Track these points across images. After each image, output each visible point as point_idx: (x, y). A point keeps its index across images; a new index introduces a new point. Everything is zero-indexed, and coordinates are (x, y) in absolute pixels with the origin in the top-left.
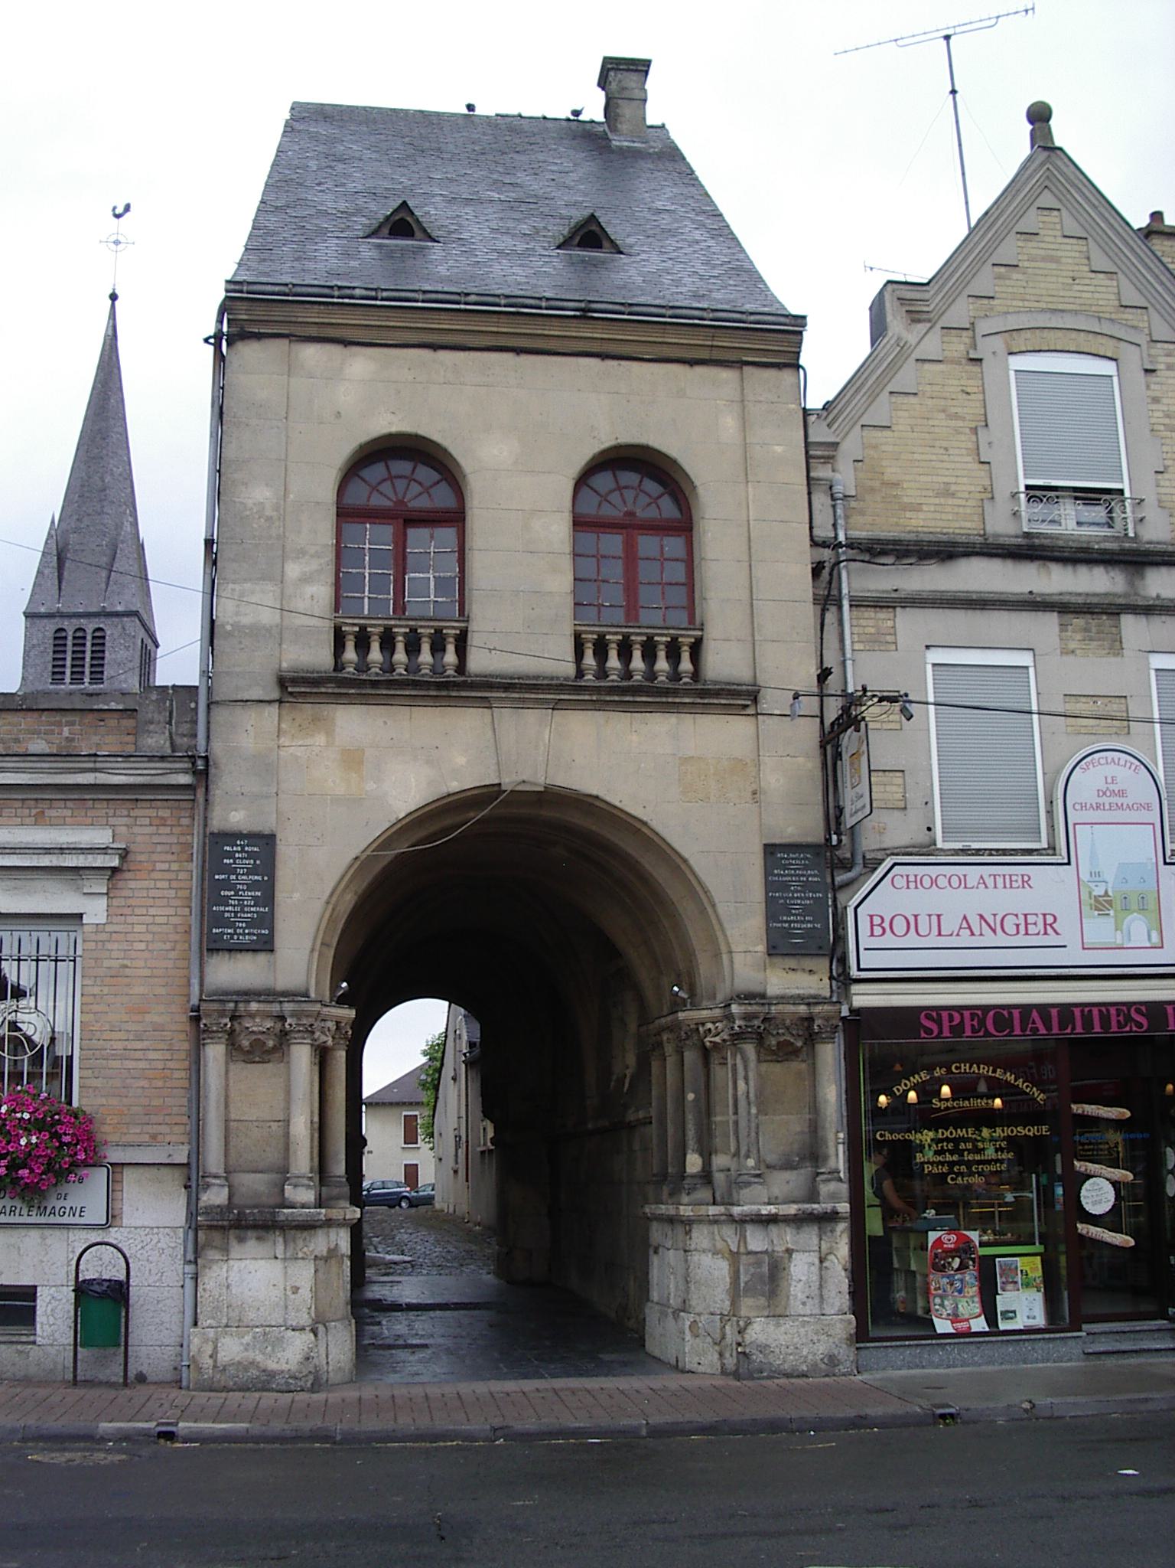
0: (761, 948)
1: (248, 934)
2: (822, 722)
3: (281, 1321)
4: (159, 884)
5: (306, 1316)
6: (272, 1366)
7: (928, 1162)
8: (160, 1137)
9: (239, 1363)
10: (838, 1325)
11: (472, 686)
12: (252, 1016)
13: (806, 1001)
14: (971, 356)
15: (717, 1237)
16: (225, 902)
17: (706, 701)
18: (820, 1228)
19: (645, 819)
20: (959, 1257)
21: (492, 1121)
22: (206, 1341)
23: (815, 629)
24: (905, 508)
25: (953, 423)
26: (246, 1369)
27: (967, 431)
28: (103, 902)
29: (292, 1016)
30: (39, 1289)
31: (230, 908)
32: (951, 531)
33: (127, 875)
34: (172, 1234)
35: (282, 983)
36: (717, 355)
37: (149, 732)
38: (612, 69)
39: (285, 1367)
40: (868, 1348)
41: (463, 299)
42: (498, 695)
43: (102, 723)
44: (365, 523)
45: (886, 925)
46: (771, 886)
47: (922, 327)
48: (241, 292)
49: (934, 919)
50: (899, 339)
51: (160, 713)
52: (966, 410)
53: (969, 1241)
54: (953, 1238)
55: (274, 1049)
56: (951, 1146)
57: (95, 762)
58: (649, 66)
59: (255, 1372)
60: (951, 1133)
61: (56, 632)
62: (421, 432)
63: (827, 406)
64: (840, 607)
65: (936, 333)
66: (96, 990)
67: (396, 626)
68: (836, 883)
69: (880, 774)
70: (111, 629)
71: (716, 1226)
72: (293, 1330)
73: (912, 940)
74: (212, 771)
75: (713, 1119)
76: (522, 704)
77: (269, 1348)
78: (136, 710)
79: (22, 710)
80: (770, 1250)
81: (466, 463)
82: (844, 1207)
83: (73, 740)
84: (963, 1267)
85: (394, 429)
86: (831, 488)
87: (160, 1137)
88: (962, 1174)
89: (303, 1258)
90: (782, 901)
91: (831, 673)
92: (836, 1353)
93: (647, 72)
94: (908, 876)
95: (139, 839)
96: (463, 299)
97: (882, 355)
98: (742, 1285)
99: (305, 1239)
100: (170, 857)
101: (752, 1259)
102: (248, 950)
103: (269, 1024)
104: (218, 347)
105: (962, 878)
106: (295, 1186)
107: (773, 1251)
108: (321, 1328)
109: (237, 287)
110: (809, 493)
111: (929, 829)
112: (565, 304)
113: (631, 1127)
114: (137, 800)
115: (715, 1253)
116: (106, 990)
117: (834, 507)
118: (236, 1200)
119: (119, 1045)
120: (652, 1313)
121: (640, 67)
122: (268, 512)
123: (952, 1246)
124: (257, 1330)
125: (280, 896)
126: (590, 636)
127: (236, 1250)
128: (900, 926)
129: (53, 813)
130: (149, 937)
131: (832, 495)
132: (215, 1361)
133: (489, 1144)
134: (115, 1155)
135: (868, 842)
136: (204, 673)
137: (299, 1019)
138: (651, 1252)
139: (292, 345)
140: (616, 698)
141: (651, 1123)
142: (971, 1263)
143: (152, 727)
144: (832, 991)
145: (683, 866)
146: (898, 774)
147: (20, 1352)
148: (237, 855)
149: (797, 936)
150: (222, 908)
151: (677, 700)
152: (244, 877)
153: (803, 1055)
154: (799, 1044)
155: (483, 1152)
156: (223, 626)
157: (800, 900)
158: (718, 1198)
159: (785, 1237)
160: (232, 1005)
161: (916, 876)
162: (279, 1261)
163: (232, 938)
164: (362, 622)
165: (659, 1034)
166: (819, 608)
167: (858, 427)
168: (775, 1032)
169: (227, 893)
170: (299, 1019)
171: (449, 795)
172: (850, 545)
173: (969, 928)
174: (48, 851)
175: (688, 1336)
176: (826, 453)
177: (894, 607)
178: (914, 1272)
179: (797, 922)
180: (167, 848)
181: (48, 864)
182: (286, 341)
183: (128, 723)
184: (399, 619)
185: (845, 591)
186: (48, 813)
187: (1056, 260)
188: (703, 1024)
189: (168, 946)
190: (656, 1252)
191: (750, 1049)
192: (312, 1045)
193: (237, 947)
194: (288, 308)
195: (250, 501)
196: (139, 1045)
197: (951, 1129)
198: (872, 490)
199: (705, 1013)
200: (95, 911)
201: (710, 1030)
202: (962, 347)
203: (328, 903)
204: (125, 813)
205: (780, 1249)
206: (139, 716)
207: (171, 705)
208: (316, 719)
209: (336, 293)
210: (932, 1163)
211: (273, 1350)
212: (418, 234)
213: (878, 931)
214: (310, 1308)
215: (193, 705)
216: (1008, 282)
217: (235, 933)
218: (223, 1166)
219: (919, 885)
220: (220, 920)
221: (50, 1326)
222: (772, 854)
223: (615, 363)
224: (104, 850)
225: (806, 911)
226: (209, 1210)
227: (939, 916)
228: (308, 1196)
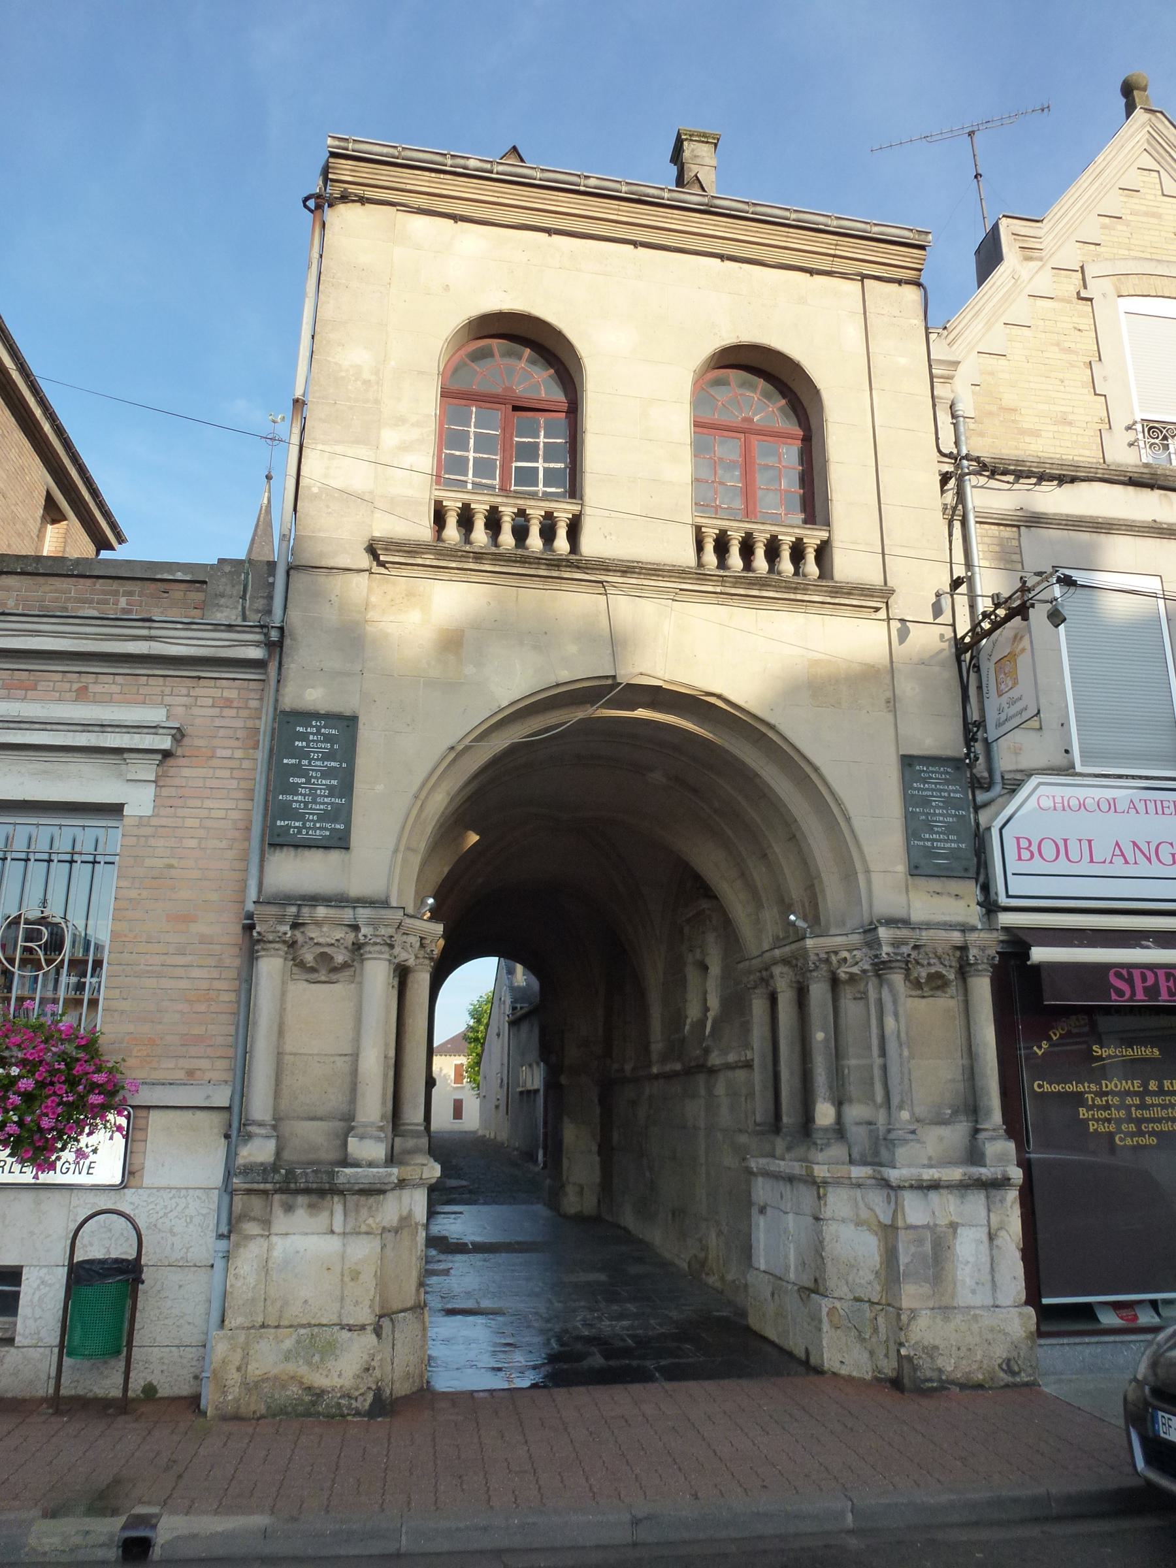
0: (901, 868)
1: (319, 828)
3: (335, 1320)
4: (219, 773)
5: (367, 1310)
6: (320, 1380)
8: (198, 1072)
9: (276, 1378)
12: (318, 924)
14: (1082, 295)
15: (861, 1205)
16: (293, 789)
17: (837, 601)
18: (987, 1197)
24: (1023, 432)
26: (284, 1387)
28: (151, 790)
30: (25, 1271)
31: (300, 798)
33: (181, 761)
34: (204, 1197)
35: (356, 889)
38: (686, 139)
43: (166, 595)
44: (469, 406)
45: (1034, 848)
46: (910, 800)
49: (1085, 845)
52: (1079, 346)
56: (1116, 1101)
57: (150, 628)
59: (294, 1390)
60: (1116, 1086)
65: (1047, 273)
66: (133, 894)
71: (859, 1190)
72: (350, 1330)
73: (1062, 866)
74: (287, 642)
75: (846, 1062)
78: (205, 582)
80: (931, 1224)
81: (583, 348)
87: (198, 1072)
89: (367, 1233)
94: (1054, 797)
95: (197, 722)
97: (998, 283)
98: (902, 1268)
101: (911, 1235)
102: (318, 847)
103: (339, 934)
106: (362, 1138)
107: (936, 1225)
111: (1067, 751)
114: (199, 678)
115: (859, 1223)
116: (145, 893)
118: (286, 1155)
122: (366, 375)
124: (302, 1331)
125: (360, 787)
126: (711, 530)
128: (1049, 850)
129: (98, 688)
130: (202, 833)
134: (145, 1097)
135: (1005, 762)
137: (376, 929)
138: (754, 1211)
140: (742, 592)
143: (222, 601)
145: (814, 776)
149: (939, 856)
150: (290, 798)
151: (806, 598)
152: (318, 763)
153: (952, 990)
156: (309, 488)
158: (855, 1155)
159: (946, 1207)
160: (293, 910)
161: (1062, 797)
162: (335, 1237)
163: (300, 832)
167: (1000, 324)
168: (925, 962)
169: (297, 780)
170: (376, 929)
171: (558, 685)
173: (1123, 855)
174: (86, 727)
175: (826, 1327)
180: (230, 732)
183: (196, 596)
186: (92, 688)
187: (1158, 216)
188: (836, 953)
189: (224, 844)
190: (762, 1210)
191: (897, 978)
192: (389, 961)
196: (181, 960)
197: (1115, 1080)
198: (991, 414)
199: (839, 940)
201: (845, 959)
203: (416, 797)
204: (184, 691)
206: (209, 588)
210: (1097, 1120)
211: (322, 1360)
213: (1026, 855)
216: (1112, 232)
217: (304, 827)
218: (271, 1112)
220: (286, 811)
221: (36, 1320)
222: (910, 765)
224: (154, 729)
225: (949, 830)
226: (247, 1170)
227: (1090, 841)
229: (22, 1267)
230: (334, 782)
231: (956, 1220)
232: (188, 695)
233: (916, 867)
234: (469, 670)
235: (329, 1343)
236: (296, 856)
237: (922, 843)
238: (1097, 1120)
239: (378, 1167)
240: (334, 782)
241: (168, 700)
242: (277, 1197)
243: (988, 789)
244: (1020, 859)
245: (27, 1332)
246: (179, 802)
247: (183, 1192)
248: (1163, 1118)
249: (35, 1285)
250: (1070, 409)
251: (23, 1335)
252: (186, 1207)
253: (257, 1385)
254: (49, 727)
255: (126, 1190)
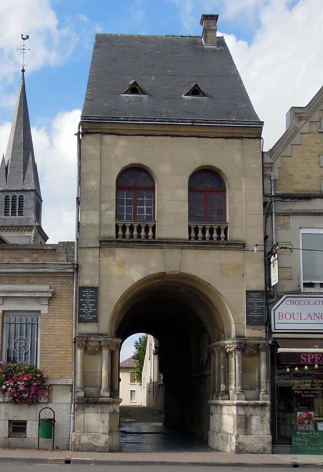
1: (90, 317)
2: (265, 252)
6: (96, 444)
7: (296, 390)
10: (266, 439)
11: (158, 242)
12: (92, 341)
13: (258, 339)
15: (230, 410)
19: (209, 283)
20: (307, 420)
21: (162, 374)
22: (77, 437)
23: (264, 223)
24: (295, 183)
25: (312, 154)
27: (317, 156)
28: (47, 307)
29: (103, 341)
30: (27, 421)
31: (85, 309)
32: (309, 190)
33: (54, 299)
36: (234, 135)
37: (60, 256)
39: (100, 445)
40: (276, 446)
41: (154, 120)
42: (165, 245)
44: (124, 191)
45: (284, 316)
47: (303, 122)
48: (86, 119)
49: (299, 314)
50: (295, 127)
51: (63, 250)
53: (310, 415)
54: (305, 414)
55: (97, 352)
58: (218, 17)
61: (6, 197)
62: (141, 163)
63: (271, 151)
64: (272, 216)
66: (45, 333)
67: (134, 224)
68: (268, 303)
69: (284, 268)
70: (26, 196)
71: (229, 407)
73: (292, 321)
74: (79, 268)
76: (171, 248)
77: (96, 439)
78: (56, 249)
79: (22, 249)
80: (245, 414)
82: (268, 402)
83: (37, 258)
84: (309, 423)
85: (133, 162)
86: (270, 177)
88: (307, 394)
89: (106, 413)
90: (251, 308)
91: (268, 237)
92: (265, 447)
93: (217, 19)
94: (291, 301)
96: (154, 120)
99: (106, 407)
100: (66, 294)
103: (96, 344)
104: (79, 137)
105: (309, 301)
107: (246, 415)
108: (111, 434)
109: (84, 118)
110: (263, 180)
111: (299, 286)
112: (186, 121)
113: (206, 376)
114: (57, 276)
117: (271, 183)
119: (51, 349)
120: (210, 434)
121: (214, 18)
123: (305, 417)
127: (86, 410)
128: (288, 316)
129: (32, 280)
130: (60, 317)
131: (271, 180)
132: (80, 443)
133: (161, 382)
136: (78, 239)
138: (211, 414)
139: (102, 136)
141: (211, 375)
142: (311, 422)
143: (61, 254)
144: (266, 336)
146: (289, 268)
147: (22, 440)
148: (87, 293)
150: (83, 309)
152: (89, 300)
154: (255, 352)
155: (159, 385)
157: (257, 307)
161: (294, 301)
163: (85, 318)
164: (124, 222)
165: (214, 347)
166: (265, 216)
169: (84, 305)
172: (276, 196)
173: (311, 317)
176: (269, 166)
177: (290, 216)
178: (293, 424)
179: (255, 314)
181: (30, 296)
182: (100, 134)
184: (135, 222)
185: (274, 211)
188: (226, 345)
190: (212, 415)
193: (87, 321)
194: (100, 124)
195: (90, 186)
196: (57, 349)
200: (44, 310)
202: (316, 128)
204: (53, 280)
205: (248, 414)
207: (66, 247)
208: (110, 252)
209: (115, 119)
210: (297, 390)
211: (97, 440)
212: (140, 92)
213: (281, 318)
214: (108, 428)
215: (73, 248)
219: (294, 304)
223: (202, 139)
224: (47, 292)
225: (258, 311)
227: (301, 313)
228: (108, 394)
229: (26, 421)
230: (93, 305)
231: (252, 414)
232: (54, 281)
233: (249, 322)
234: (126, 273)
235: (98, 436)
236: (85, 324)
237: (250, 315)
238: (297, 390)
239: (108, 398)
240: (93, 305)
241: (49, 283)
242: (85, 404)
243: (273, 298)
244: (279, 319)
245: (29, 435)
246: (54, 310)
247: (62, 404)
248: (317, 390)
249: (30, 424)
250: (311, 173)
251: (28, 435)
252: (63, 407)
253: (82, 445)
254: (21, 292)
255: (49, 404)
